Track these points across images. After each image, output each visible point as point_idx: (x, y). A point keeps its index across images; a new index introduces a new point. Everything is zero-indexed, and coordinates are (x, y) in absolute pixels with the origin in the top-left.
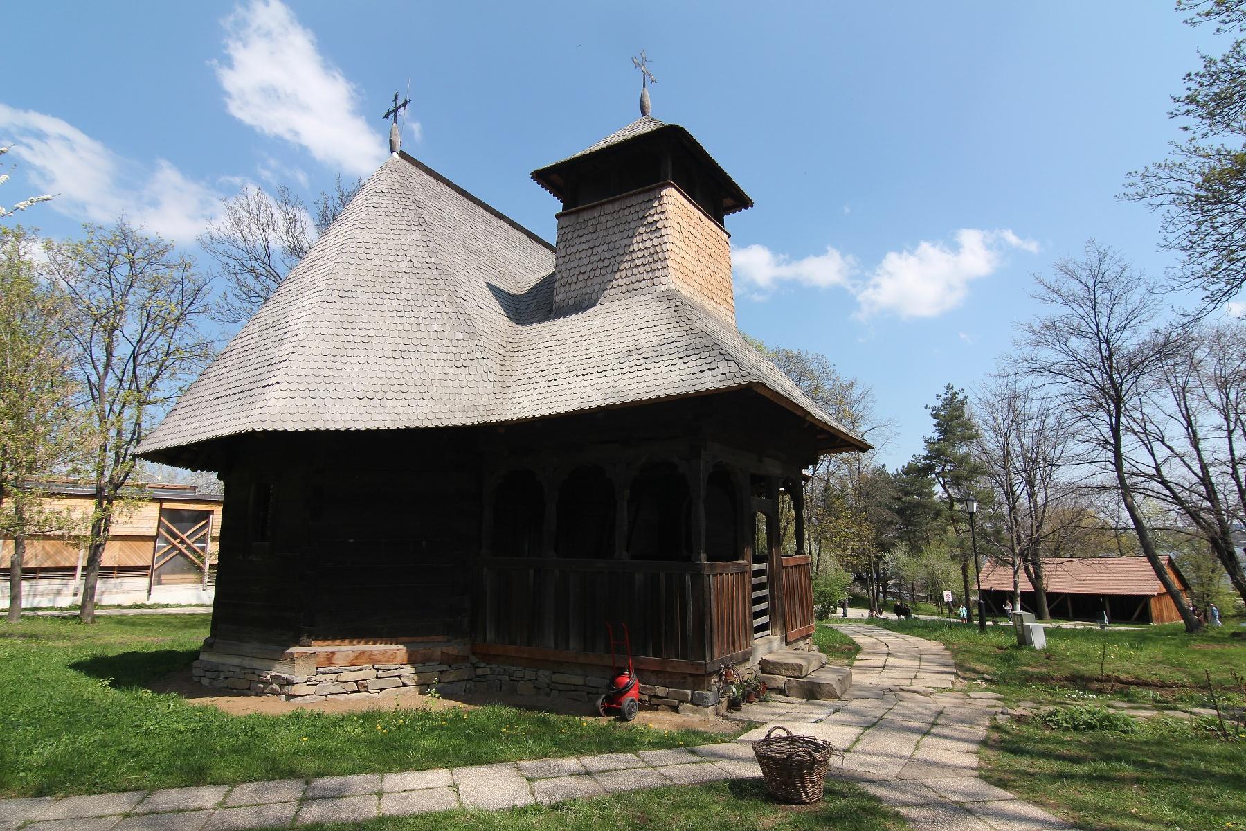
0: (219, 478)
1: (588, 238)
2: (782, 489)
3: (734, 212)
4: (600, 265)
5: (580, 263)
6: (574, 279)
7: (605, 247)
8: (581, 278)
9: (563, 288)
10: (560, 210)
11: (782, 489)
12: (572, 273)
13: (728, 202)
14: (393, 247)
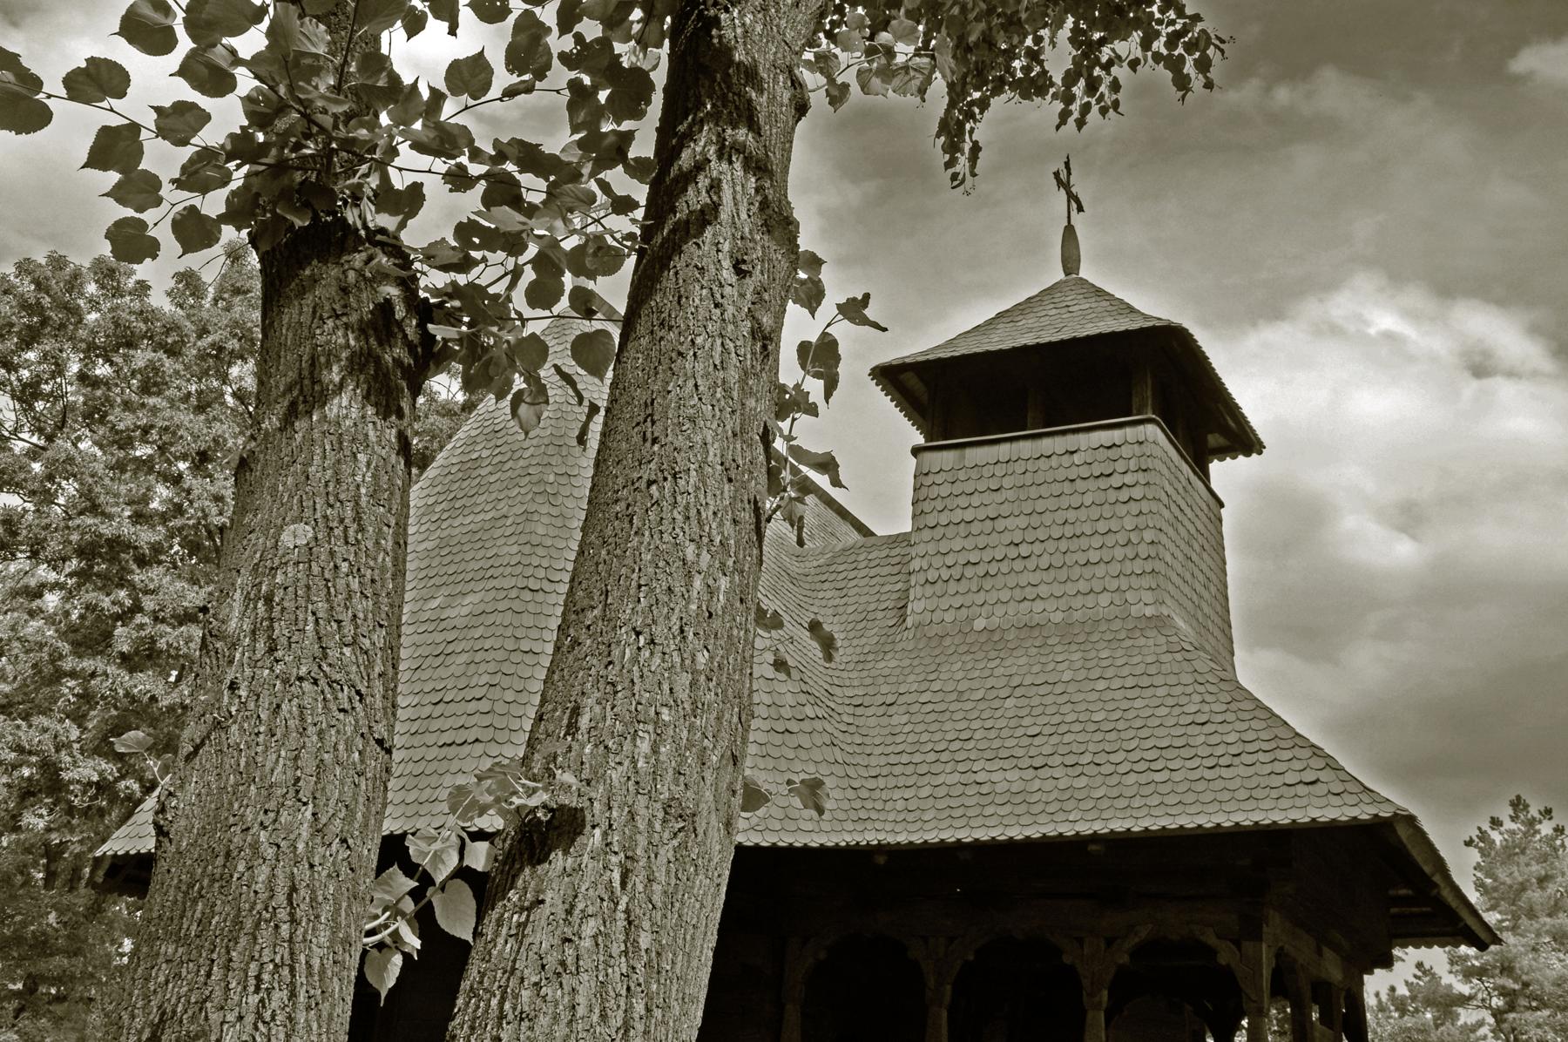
2: (476, 240)
3: (1234, 458)
4: (1013, 552)
5: (969, 543)
6: (956, 572)
7: (1022, 522)
8: (969, 572)
9: (929, 590)
10: (445, 25)
11: (476, 240)
12: (950, 560)
13: (1214, 440)
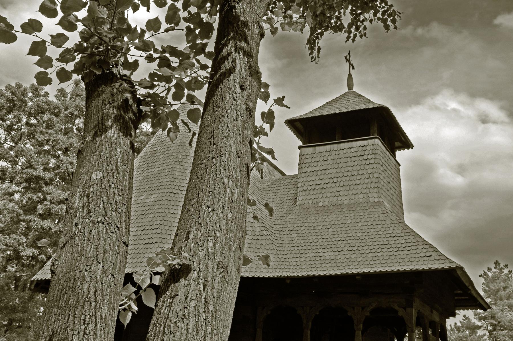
0: (449, 318)
1: (323, 163)
3: (404, 150)
4: (331, 181)
5: (317, 178)
6: (313, 187)
7: (334, 171)
8: (317, 187)
9: (304, 193)
12: (311, 183)
13: (397, 144)
14: (405, 256)
